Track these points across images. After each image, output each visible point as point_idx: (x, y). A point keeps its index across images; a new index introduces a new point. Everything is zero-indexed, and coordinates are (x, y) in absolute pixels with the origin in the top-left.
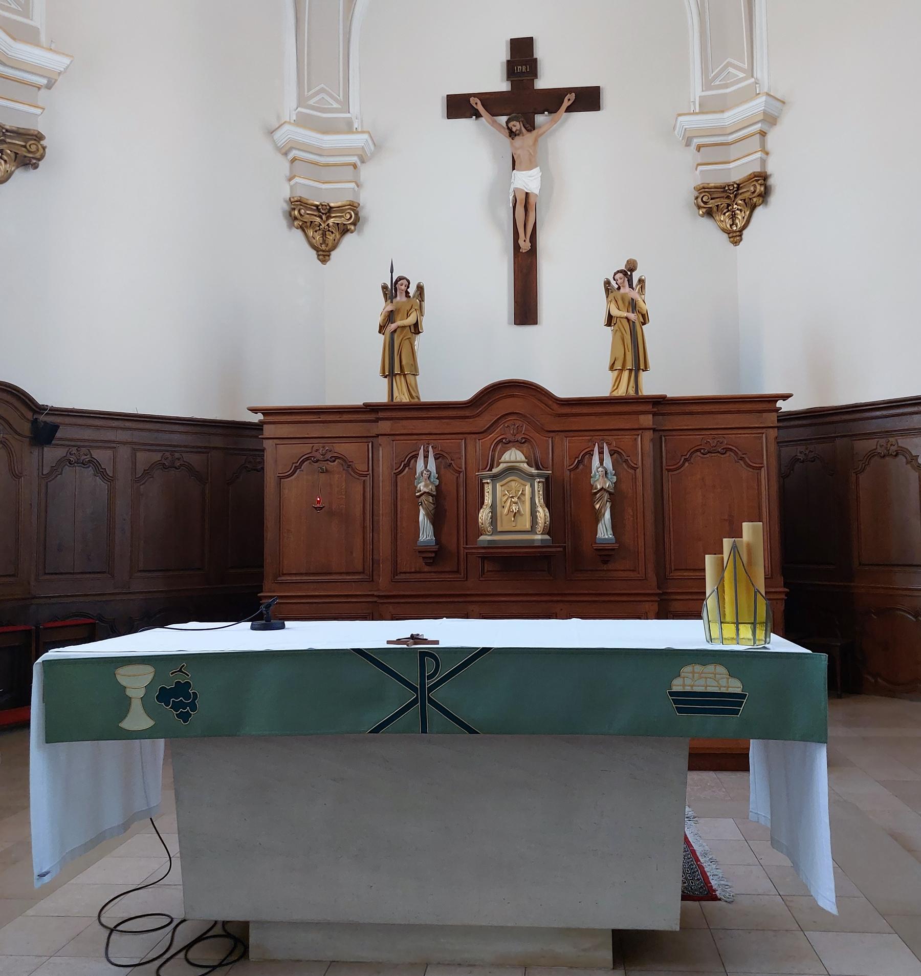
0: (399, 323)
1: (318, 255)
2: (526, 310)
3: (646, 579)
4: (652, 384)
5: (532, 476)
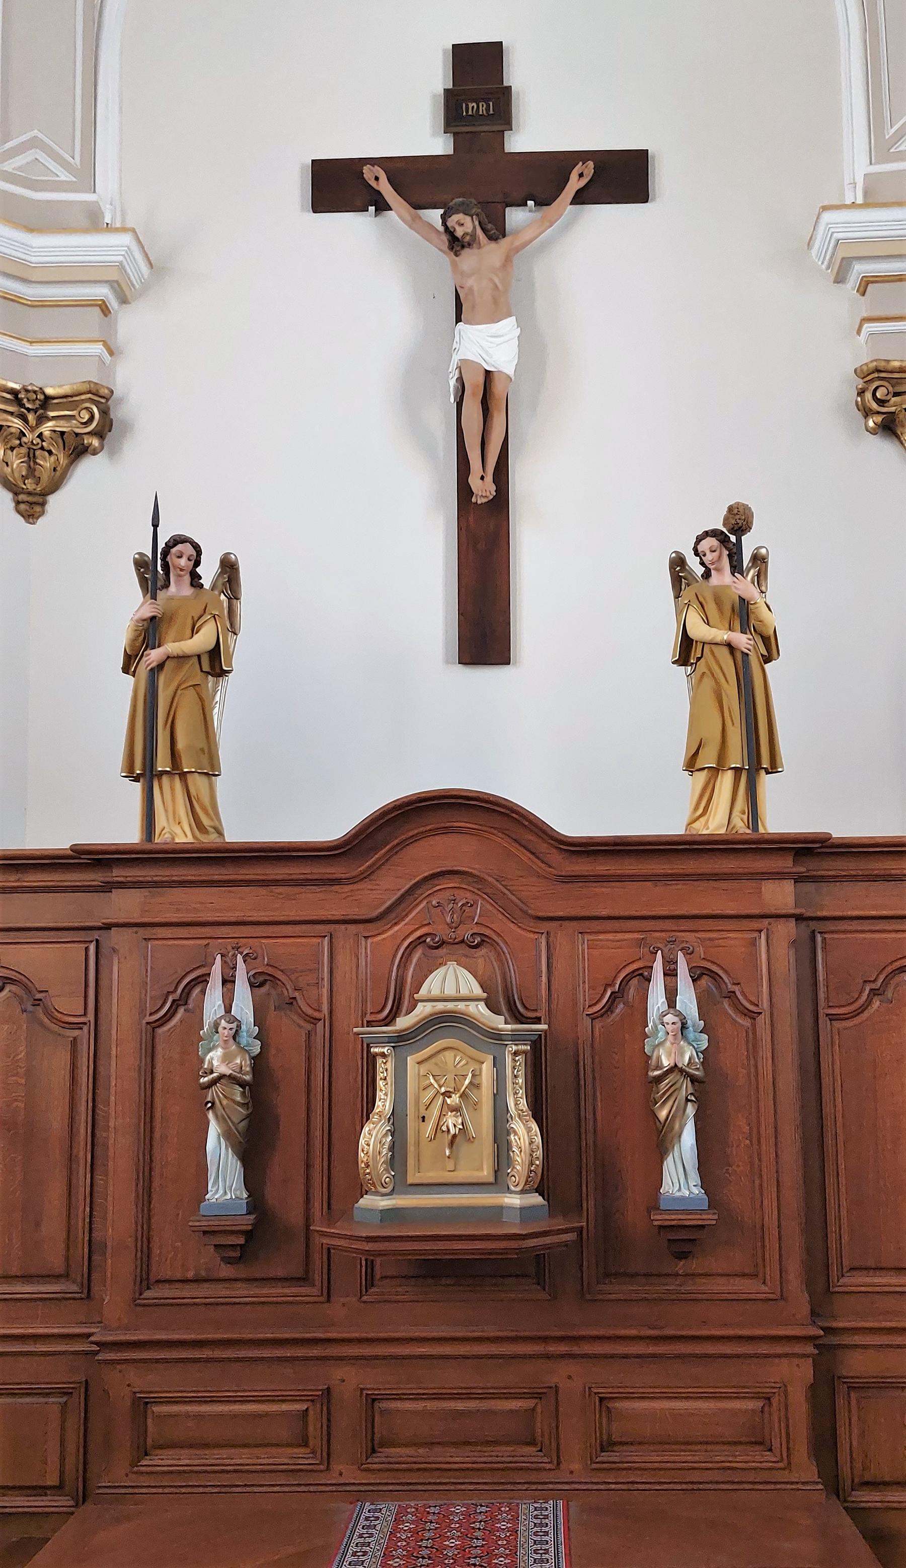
0: (171, 647)
1: (18, 503)
2: (484, 634)
3: (782, 1298)
4: (789, 808)
5: (497, 1037)
